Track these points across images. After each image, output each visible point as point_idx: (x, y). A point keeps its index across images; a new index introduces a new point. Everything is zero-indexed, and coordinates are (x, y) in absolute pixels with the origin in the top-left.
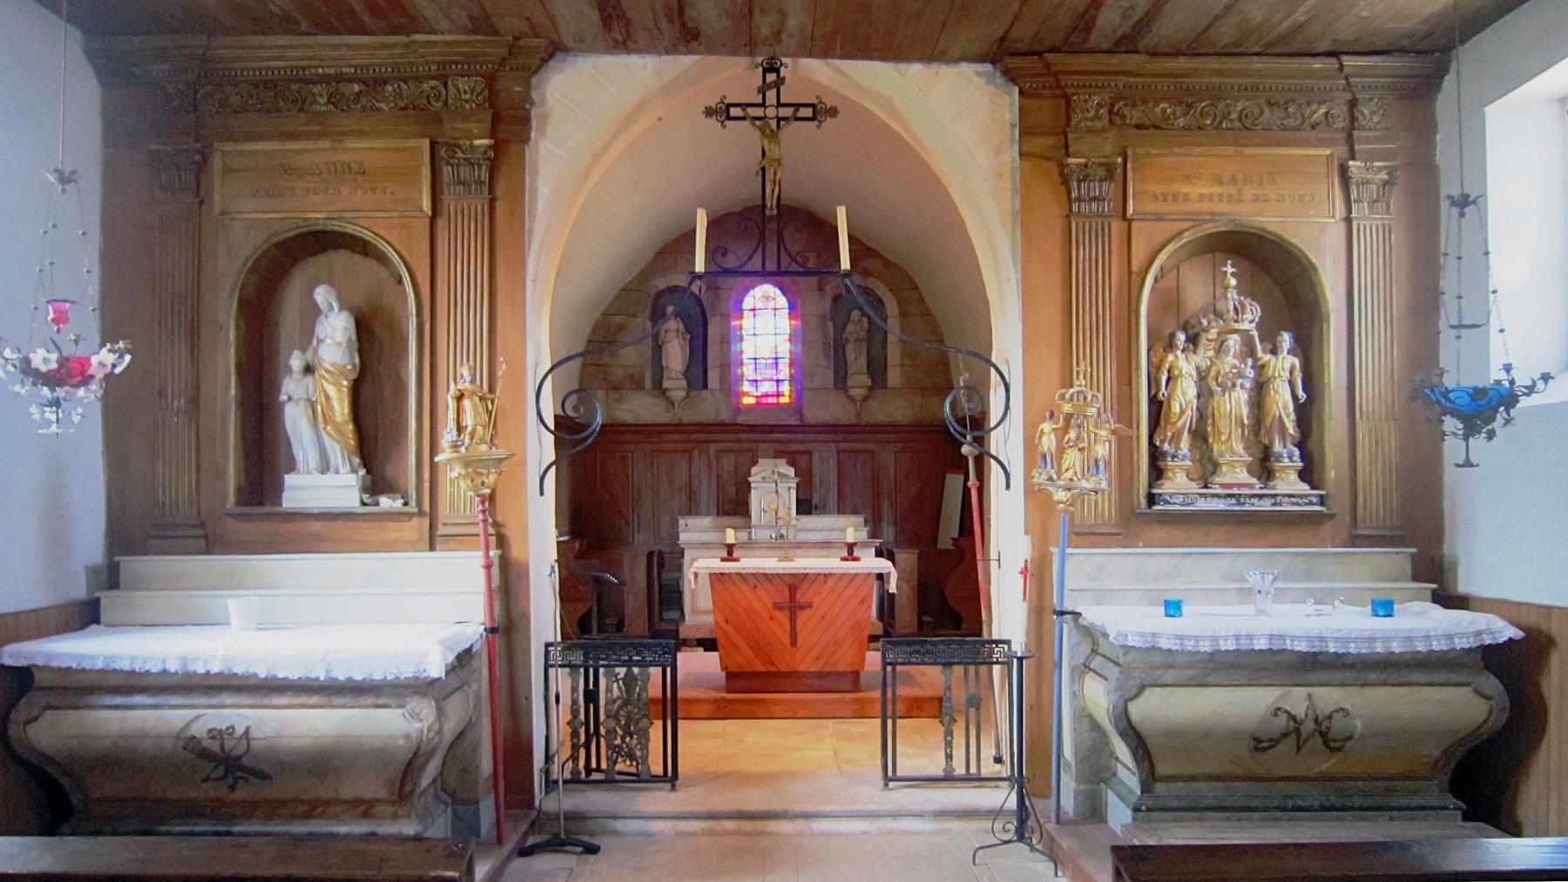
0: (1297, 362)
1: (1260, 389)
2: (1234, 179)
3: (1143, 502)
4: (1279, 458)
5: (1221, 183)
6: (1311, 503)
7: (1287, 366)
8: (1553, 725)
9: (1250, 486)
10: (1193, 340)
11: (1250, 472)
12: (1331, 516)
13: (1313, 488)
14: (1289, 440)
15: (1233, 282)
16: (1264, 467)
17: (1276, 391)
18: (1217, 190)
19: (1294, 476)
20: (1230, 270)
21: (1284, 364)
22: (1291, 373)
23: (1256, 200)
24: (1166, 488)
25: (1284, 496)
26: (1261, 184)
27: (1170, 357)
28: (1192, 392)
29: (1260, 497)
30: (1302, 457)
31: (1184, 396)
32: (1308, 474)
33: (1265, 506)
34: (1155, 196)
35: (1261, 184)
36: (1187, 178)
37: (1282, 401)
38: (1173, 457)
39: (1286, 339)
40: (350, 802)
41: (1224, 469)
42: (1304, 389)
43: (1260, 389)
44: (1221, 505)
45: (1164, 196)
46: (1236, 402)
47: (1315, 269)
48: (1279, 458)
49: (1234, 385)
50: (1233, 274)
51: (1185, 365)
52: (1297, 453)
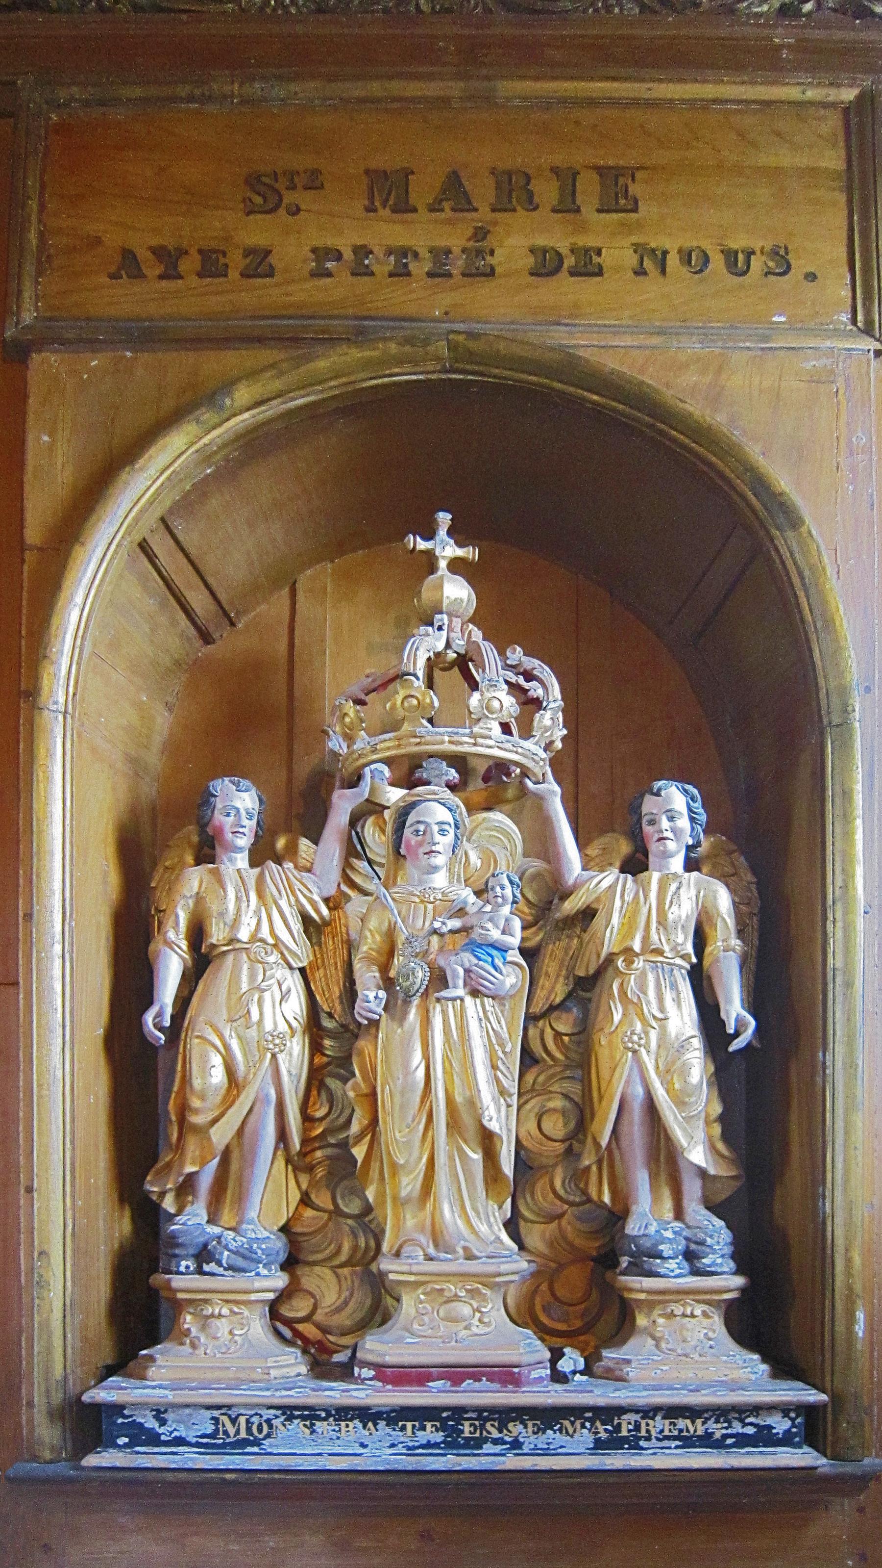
0: (724, 900)
1: (572, 992)
2: (454, 193)
3: (47, 1434)
4: (644, 1259)
5: (404, 208)
6: (765, 1438)
7: (684, 909)
8: (862, 714)
9: (507, 1375)
10: (297, 813)
11: (525, 1315)
12: (858, 1483)
13: (784, 1367)
14: (693, 1189)
15: (457, 591)
16: (586, 1291)
17: (630, 1004)
18: (386, 232)
19: (706, 1328)
20: (447, 550)
21: (673, 902)
22: (700, 941)
23: (547, 265)
24: (167, 1374)
25: (649, 1412)
26: (567, 206)
27: (194, 879)
28: (281, 1008)
29: (548, 1417)
30: (744, 1258)
31: (250, 1035)
32: (774, 1312)
33: (573, 1452)
34: (128, 257)
35: (567, 206)
36: (266, 193)
37: (661, 1047)
38: (204, 1255)
39: (675, 810)
40: (241, 1175)
41: (408, 1304)
42: (756, 1003)
43: (572, 992)
44: (379, 1451)
45: (169, 260)
46: (461, 1053)
47: (795, 522)
48: (644, 1259)
49: (440, 979)
50: (456, 566)
51: (253, 908)
52: (718, 1235)
